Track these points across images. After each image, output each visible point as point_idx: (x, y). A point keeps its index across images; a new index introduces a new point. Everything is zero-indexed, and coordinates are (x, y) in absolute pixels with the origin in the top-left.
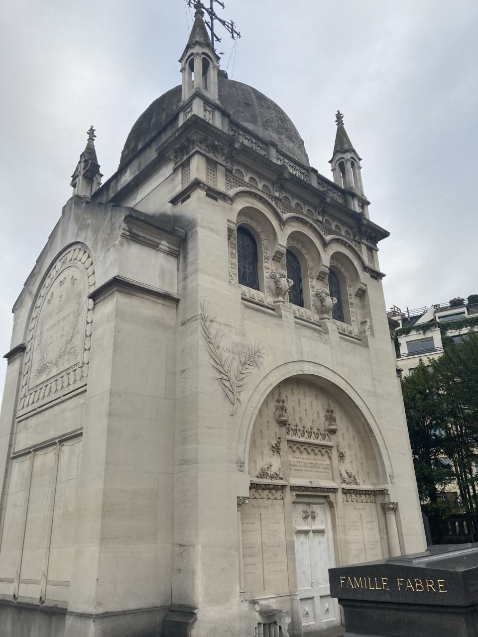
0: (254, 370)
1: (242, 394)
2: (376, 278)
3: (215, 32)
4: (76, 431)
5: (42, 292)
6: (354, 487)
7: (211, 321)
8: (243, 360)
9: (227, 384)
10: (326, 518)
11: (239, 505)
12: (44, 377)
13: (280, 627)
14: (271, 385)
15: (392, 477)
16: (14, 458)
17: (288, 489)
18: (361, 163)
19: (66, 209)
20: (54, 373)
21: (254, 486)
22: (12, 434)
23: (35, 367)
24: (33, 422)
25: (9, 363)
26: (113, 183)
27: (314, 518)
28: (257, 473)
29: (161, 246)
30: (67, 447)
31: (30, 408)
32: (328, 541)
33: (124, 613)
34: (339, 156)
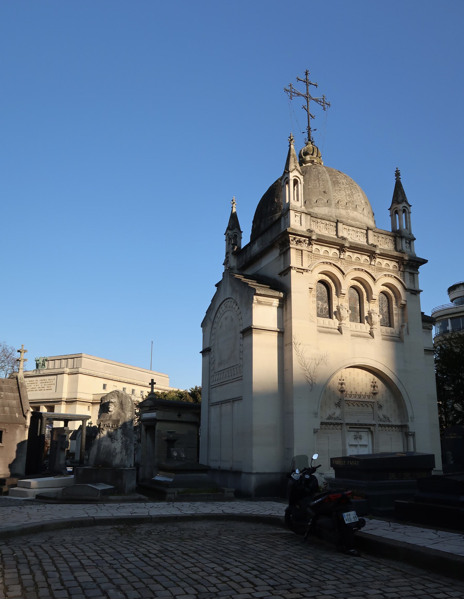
2: (415, 294)
3: (310, 112)
4: (240, 397)
5: (216, 320)
6: (388, 423)
10: (368, 439)
11: (314, 432)
12: (222, 368)
15: (413, 418)
16: (211, 406)
18: (412, 209)
19: (225, 275)
20: (226, 366)
21: (322, 424)
22: (209, 394)
23: (217, 362)
24: (218, 389)
25: (203, 356)
26: (249, 248)
27: (361, 438)
28: (327, 418)
29: (273, 304)
30: (236, 404)
31: (217, 382)
32: (369, 450)
33: (264, 473)
34: (395, 206)
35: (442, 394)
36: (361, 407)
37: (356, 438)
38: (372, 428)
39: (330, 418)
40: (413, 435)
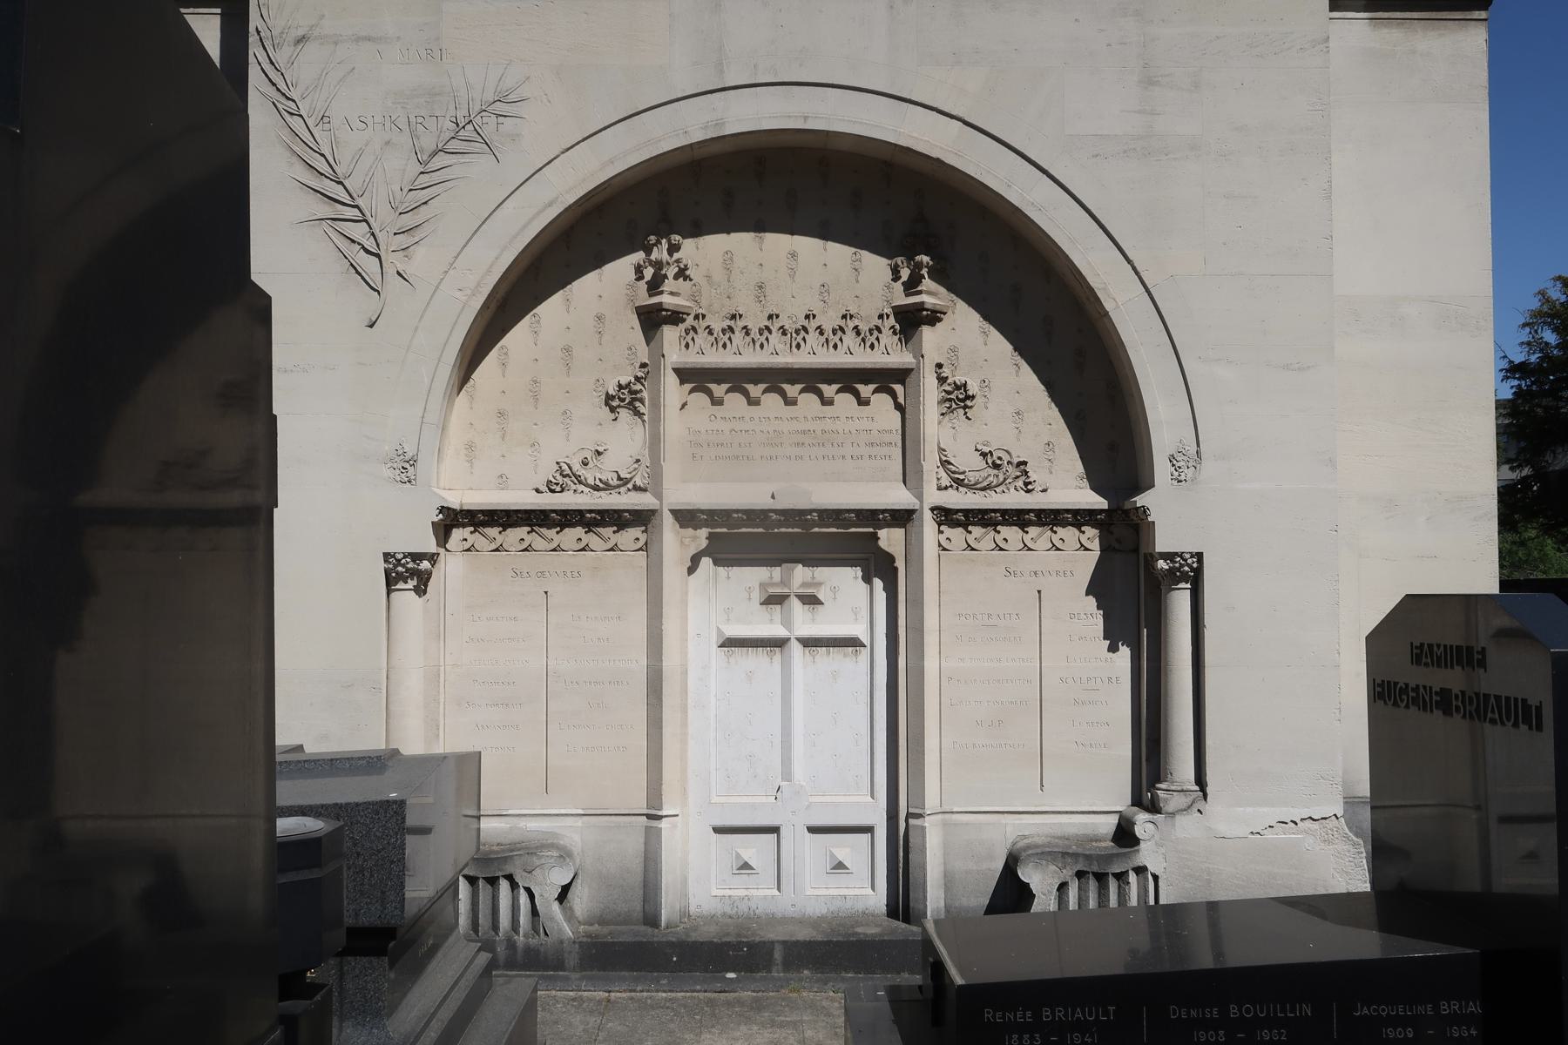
0: (480, 164)
1: (419, 253)
6: (1013, 499)
7: (301, 40)
8: (428, 143)
9: (358, 231)
13: (528, 890)
14: (550, 204)
17: (668, 521)
35: (1501, 566)
36: (773, 400)
37: (774, 600)
38: (890, 539)
39: (566, 477)
40: (1192, 573)
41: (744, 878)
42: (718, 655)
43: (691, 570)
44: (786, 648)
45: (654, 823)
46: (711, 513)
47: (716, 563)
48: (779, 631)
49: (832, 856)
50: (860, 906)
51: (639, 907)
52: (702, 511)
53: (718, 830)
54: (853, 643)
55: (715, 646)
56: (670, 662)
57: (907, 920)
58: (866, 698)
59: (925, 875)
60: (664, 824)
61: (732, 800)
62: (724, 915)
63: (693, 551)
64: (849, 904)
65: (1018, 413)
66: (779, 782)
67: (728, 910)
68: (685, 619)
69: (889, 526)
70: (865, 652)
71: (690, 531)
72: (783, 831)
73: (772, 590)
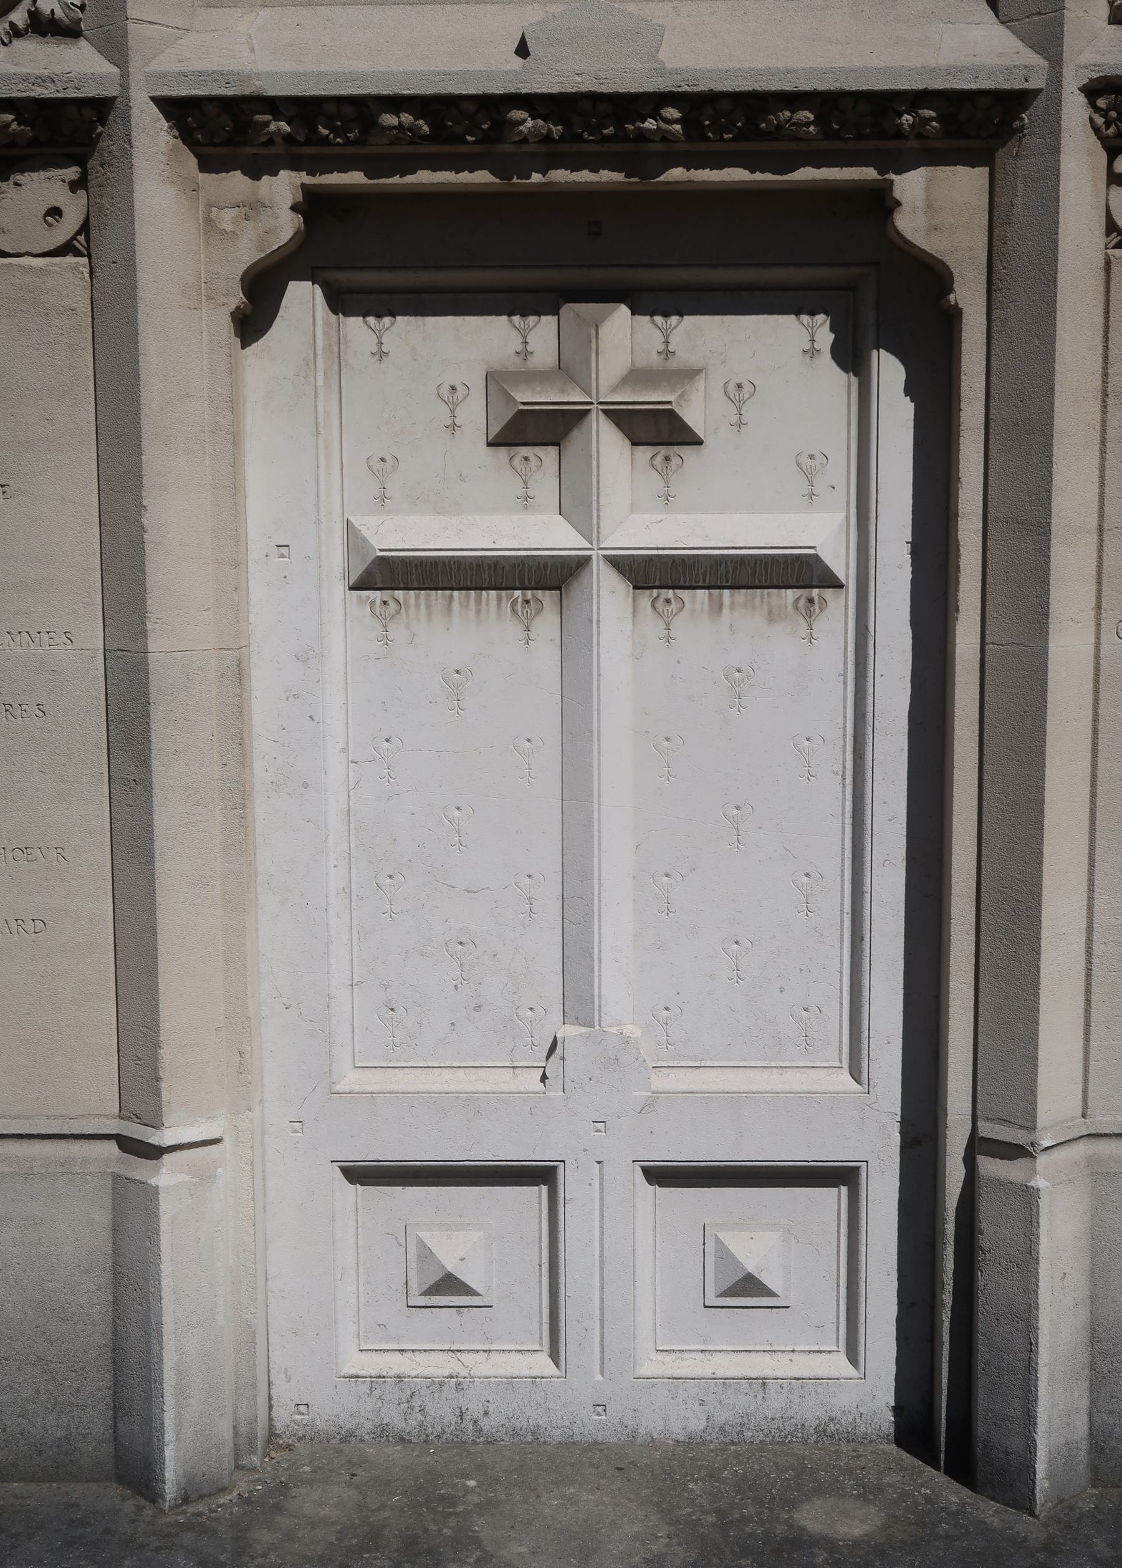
17: (151, 141)
37: (536, 429)
38: (937, 206)
41: (443, 1320)
42: (348, 618)
43: (253, 320)
44: (575, 591)
45: (138, 1169)
46: (306, 110)
47: (341, 301)
48: (548, 534)
49: (724, 1255)
50: (810, 1411)
51: (100, 1426)
52: (273, 105)
53: (360, 1174)
54: (800, 573)
55: (339, 588)
56: (177, 637)
57: (963, 1465)
58: (835, 758)
59: (1031, 1347)
60: (166, 1176)
61: (405, 1081)
62: (382, 1432)
63: (247, 252)
64: (775, 1404)
65: (453, 1024)
66: (553, 1025)
67: (393, 1417)
68: (233, 487)
69: (935, 157)
70: (838, 610)
71: (236, 182)
72: (570, 1182)
73: (526, 396)
